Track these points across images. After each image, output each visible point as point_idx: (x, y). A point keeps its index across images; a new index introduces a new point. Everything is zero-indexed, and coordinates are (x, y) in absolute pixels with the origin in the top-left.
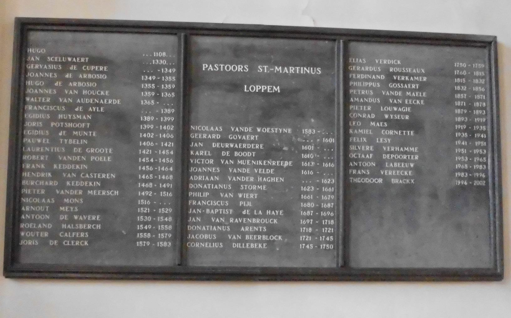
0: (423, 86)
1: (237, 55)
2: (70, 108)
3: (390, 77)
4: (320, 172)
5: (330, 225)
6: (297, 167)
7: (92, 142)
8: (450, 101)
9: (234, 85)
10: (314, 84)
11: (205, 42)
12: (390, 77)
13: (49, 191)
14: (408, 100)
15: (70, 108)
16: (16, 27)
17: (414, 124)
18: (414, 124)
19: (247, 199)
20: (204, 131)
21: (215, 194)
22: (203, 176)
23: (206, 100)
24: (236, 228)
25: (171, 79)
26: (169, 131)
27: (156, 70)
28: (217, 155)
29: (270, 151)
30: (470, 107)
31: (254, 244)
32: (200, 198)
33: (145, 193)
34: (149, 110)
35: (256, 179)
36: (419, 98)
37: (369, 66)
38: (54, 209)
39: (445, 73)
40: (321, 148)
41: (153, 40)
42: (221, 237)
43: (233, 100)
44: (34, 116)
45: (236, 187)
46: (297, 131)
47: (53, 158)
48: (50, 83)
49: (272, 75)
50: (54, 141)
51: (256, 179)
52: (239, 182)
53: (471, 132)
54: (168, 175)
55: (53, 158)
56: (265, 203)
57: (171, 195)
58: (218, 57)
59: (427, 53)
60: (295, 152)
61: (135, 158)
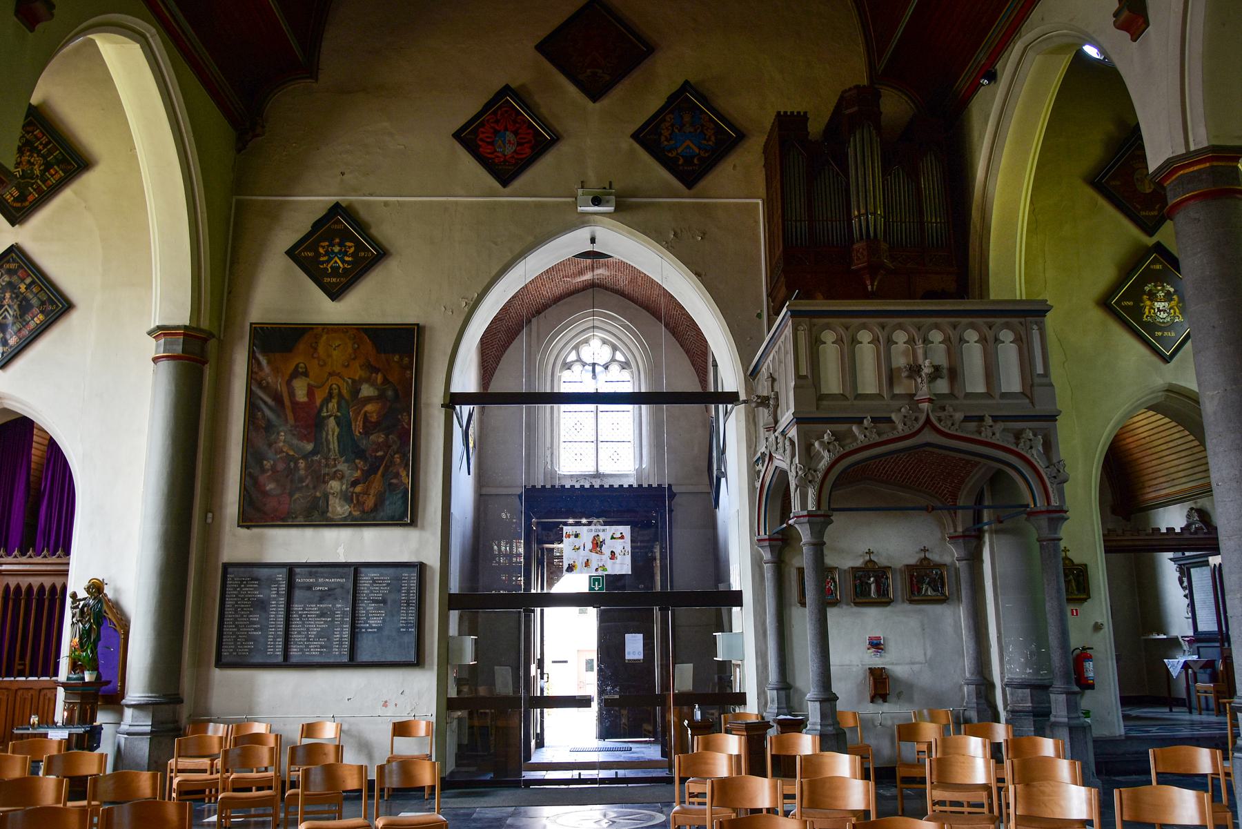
0: (388, 585)
1: (311, 575)
2: (243, 599)
3: (374, 581)
4: (342, 622)
5: (346, 644)
6: (333, 621)
7: (251, 613)
8: (399, 591)
9: (309, 588)
10: (342, 586)
11: (298, 570)
12: (374, 581)
13: (234, 633)
14: (380, 591)
15: (243, 599)
16: (388, 247)
17: (384, 601)
18: (384, 601)
19: (312, 634)
20: (297, 607)
21: (299, 633)
22: (296, 625)
23: (298, 594)
24: (307, 646)
25: (283, 587)
26: (282, 607)
27: (277, 582)
28: (300, 616)
29: (322, 615)
30: (408, 592)
31: (314, 653)
32: (295, 636)
33: (271, 632)
34: (274, 599)
35: (316, 626)
36: (386, 590)
37: (367, 577)
38: (235, 640)
39: (399, 579)
40: (344, 613)
41: (277, 570)
42: (301, 650)
43: (308, 594)
44: (229, 603)
45: (308, 629)
46: (334, 605)
47: (236, 619)
48: (235, 589)
49: (324, 582)
50: (236, 612)
51: (316, 626)
52: (311, 625)
53: (408, 604)
54: (281, 626)
55: (236, 619)
56: (319, 636)
57: (658, 589)
58: (303, 576)
59: (391, 571)
60: (333, 614)
61: (268, 619)
